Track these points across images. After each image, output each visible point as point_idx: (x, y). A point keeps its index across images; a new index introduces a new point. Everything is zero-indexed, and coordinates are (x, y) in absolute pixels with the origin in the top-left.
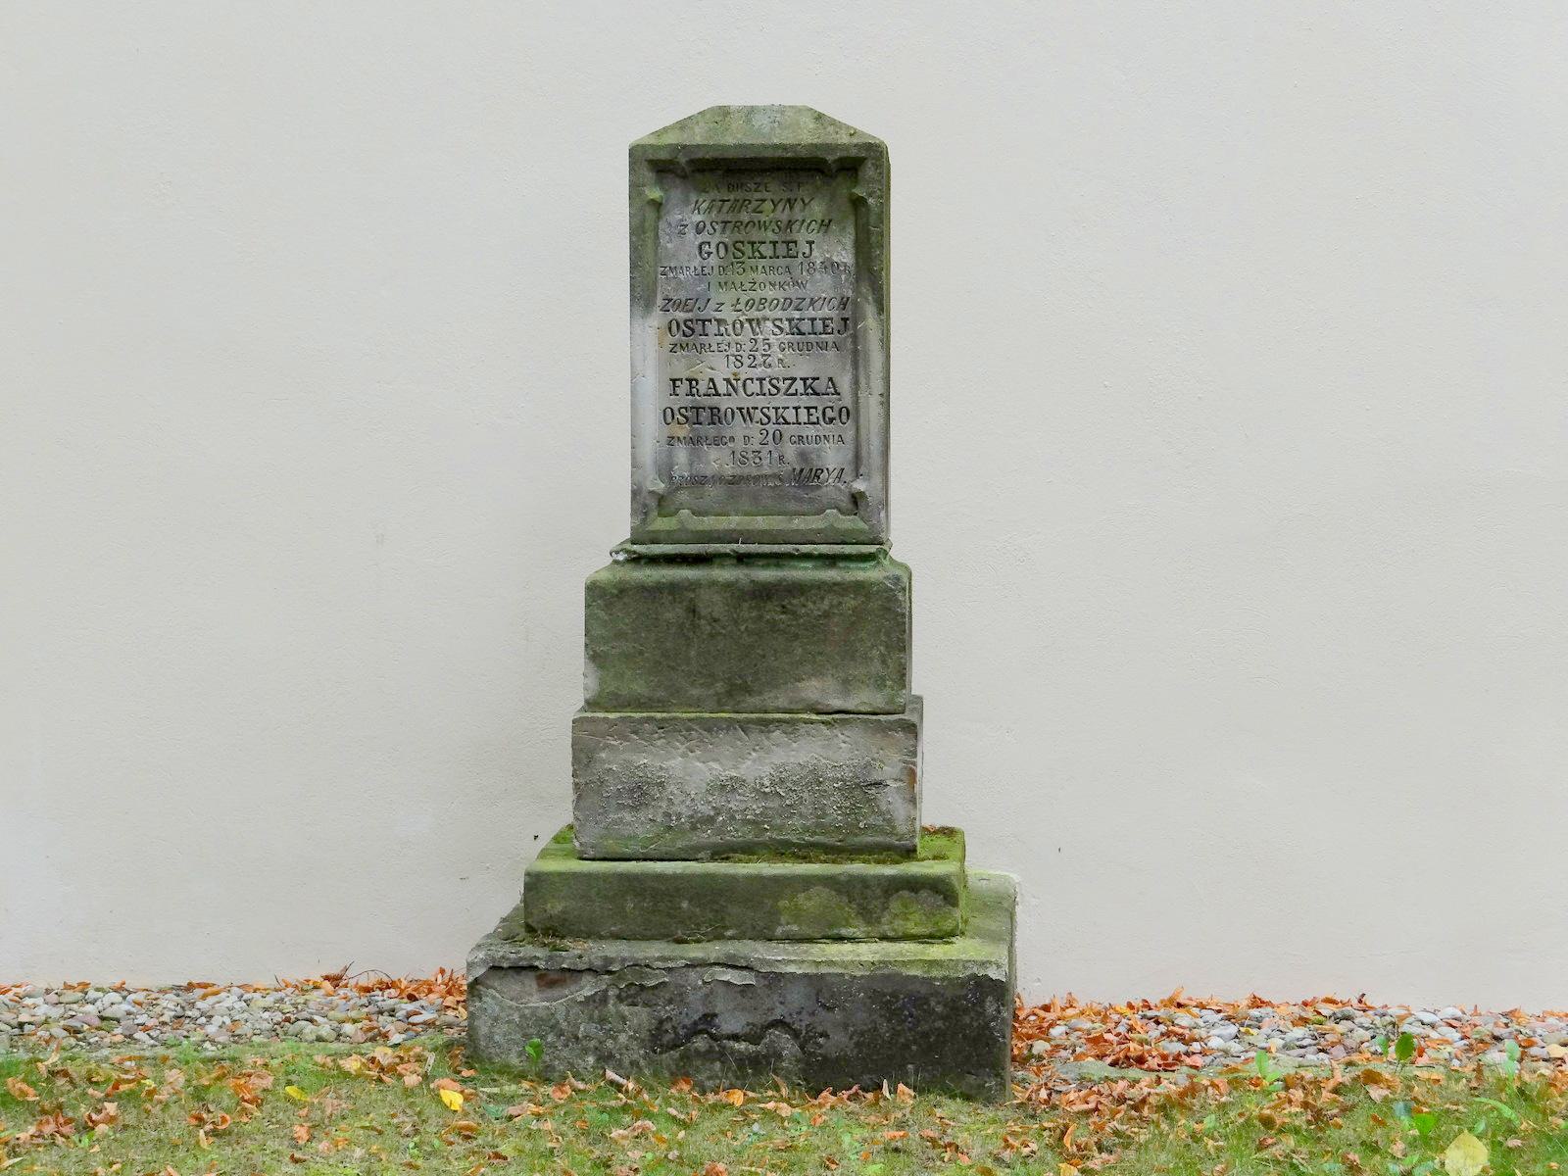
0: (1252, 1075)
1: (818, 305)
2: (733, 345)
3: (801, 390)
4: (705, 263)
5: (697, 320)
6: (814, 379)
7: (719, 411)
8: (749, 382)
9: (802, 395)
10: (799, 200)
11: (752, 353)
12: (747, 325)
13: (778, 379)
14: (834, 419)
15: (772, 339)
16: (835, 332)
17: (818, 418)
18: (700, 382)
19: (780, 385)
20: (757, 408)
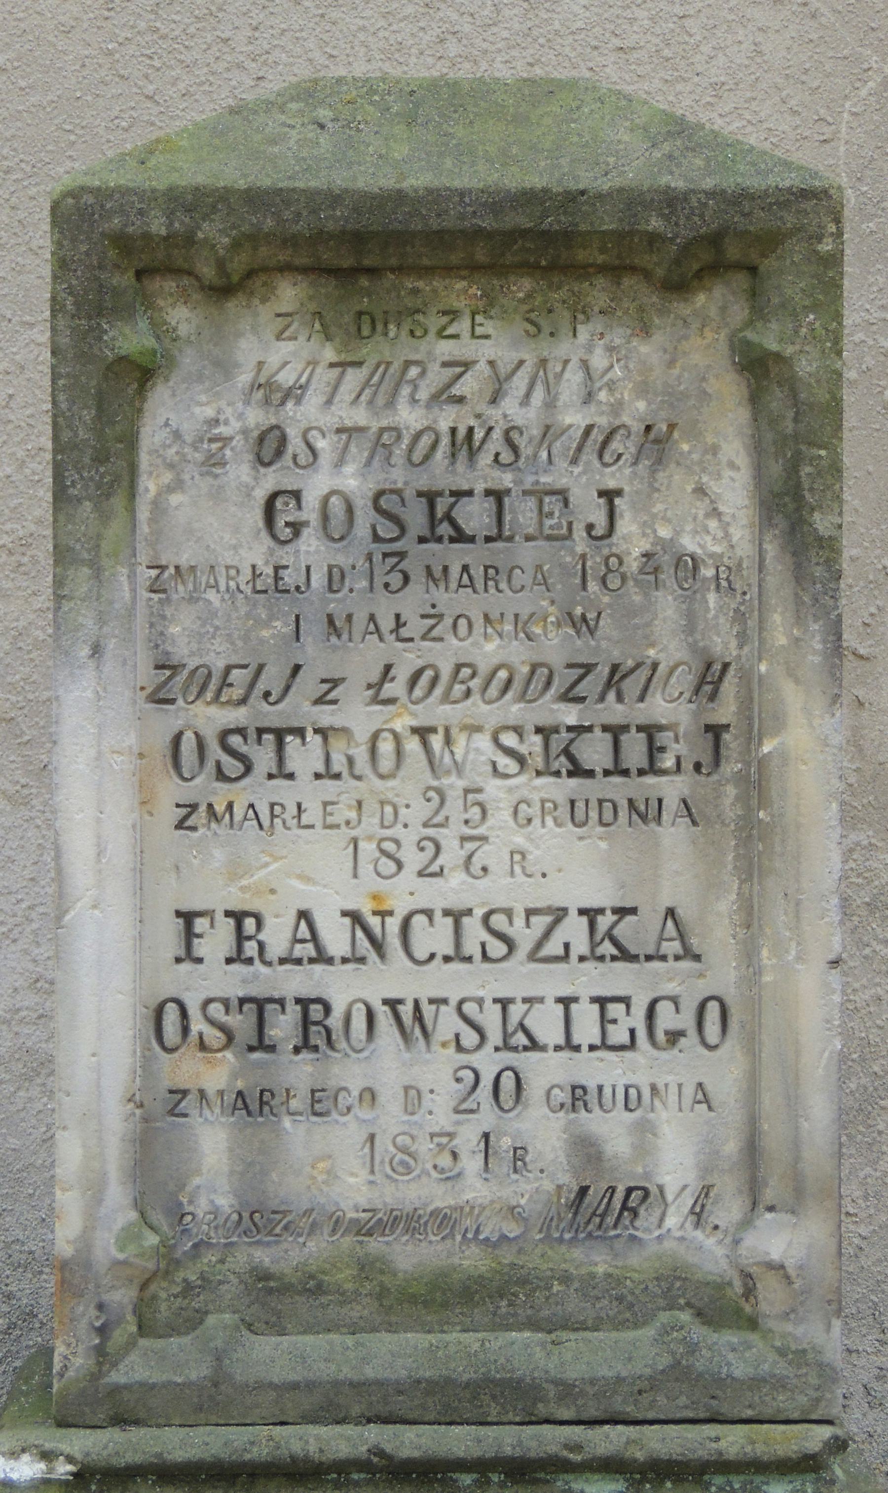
0: (672, 830)
1: (632, 687)
2: (370, 806)
3: (581, 946)
4: (285, 556)
5: (260, 731)
6: (622, 912)
7: (327, 1009)
8: (419, 920)
9: (582, 959)
10: (574, 364)
11: (431, 832)
12: (413, 745)
13: (509, 913)
14: (681, 1034)
15: (494, 788)
16: (687, 765)
17: (632, 1032)
18: (269, 922)
19: (518, 929)
20: (445, 1001)
